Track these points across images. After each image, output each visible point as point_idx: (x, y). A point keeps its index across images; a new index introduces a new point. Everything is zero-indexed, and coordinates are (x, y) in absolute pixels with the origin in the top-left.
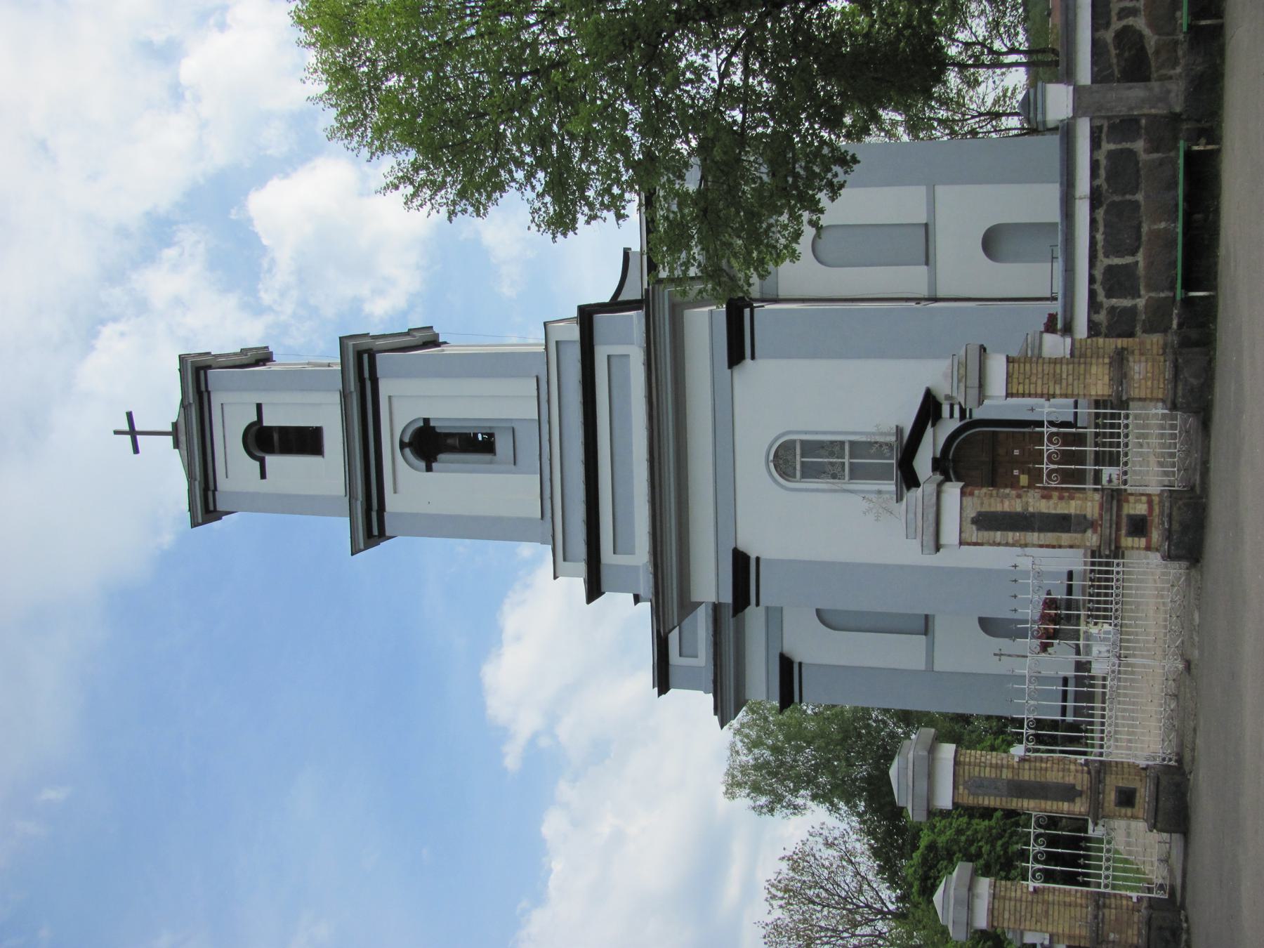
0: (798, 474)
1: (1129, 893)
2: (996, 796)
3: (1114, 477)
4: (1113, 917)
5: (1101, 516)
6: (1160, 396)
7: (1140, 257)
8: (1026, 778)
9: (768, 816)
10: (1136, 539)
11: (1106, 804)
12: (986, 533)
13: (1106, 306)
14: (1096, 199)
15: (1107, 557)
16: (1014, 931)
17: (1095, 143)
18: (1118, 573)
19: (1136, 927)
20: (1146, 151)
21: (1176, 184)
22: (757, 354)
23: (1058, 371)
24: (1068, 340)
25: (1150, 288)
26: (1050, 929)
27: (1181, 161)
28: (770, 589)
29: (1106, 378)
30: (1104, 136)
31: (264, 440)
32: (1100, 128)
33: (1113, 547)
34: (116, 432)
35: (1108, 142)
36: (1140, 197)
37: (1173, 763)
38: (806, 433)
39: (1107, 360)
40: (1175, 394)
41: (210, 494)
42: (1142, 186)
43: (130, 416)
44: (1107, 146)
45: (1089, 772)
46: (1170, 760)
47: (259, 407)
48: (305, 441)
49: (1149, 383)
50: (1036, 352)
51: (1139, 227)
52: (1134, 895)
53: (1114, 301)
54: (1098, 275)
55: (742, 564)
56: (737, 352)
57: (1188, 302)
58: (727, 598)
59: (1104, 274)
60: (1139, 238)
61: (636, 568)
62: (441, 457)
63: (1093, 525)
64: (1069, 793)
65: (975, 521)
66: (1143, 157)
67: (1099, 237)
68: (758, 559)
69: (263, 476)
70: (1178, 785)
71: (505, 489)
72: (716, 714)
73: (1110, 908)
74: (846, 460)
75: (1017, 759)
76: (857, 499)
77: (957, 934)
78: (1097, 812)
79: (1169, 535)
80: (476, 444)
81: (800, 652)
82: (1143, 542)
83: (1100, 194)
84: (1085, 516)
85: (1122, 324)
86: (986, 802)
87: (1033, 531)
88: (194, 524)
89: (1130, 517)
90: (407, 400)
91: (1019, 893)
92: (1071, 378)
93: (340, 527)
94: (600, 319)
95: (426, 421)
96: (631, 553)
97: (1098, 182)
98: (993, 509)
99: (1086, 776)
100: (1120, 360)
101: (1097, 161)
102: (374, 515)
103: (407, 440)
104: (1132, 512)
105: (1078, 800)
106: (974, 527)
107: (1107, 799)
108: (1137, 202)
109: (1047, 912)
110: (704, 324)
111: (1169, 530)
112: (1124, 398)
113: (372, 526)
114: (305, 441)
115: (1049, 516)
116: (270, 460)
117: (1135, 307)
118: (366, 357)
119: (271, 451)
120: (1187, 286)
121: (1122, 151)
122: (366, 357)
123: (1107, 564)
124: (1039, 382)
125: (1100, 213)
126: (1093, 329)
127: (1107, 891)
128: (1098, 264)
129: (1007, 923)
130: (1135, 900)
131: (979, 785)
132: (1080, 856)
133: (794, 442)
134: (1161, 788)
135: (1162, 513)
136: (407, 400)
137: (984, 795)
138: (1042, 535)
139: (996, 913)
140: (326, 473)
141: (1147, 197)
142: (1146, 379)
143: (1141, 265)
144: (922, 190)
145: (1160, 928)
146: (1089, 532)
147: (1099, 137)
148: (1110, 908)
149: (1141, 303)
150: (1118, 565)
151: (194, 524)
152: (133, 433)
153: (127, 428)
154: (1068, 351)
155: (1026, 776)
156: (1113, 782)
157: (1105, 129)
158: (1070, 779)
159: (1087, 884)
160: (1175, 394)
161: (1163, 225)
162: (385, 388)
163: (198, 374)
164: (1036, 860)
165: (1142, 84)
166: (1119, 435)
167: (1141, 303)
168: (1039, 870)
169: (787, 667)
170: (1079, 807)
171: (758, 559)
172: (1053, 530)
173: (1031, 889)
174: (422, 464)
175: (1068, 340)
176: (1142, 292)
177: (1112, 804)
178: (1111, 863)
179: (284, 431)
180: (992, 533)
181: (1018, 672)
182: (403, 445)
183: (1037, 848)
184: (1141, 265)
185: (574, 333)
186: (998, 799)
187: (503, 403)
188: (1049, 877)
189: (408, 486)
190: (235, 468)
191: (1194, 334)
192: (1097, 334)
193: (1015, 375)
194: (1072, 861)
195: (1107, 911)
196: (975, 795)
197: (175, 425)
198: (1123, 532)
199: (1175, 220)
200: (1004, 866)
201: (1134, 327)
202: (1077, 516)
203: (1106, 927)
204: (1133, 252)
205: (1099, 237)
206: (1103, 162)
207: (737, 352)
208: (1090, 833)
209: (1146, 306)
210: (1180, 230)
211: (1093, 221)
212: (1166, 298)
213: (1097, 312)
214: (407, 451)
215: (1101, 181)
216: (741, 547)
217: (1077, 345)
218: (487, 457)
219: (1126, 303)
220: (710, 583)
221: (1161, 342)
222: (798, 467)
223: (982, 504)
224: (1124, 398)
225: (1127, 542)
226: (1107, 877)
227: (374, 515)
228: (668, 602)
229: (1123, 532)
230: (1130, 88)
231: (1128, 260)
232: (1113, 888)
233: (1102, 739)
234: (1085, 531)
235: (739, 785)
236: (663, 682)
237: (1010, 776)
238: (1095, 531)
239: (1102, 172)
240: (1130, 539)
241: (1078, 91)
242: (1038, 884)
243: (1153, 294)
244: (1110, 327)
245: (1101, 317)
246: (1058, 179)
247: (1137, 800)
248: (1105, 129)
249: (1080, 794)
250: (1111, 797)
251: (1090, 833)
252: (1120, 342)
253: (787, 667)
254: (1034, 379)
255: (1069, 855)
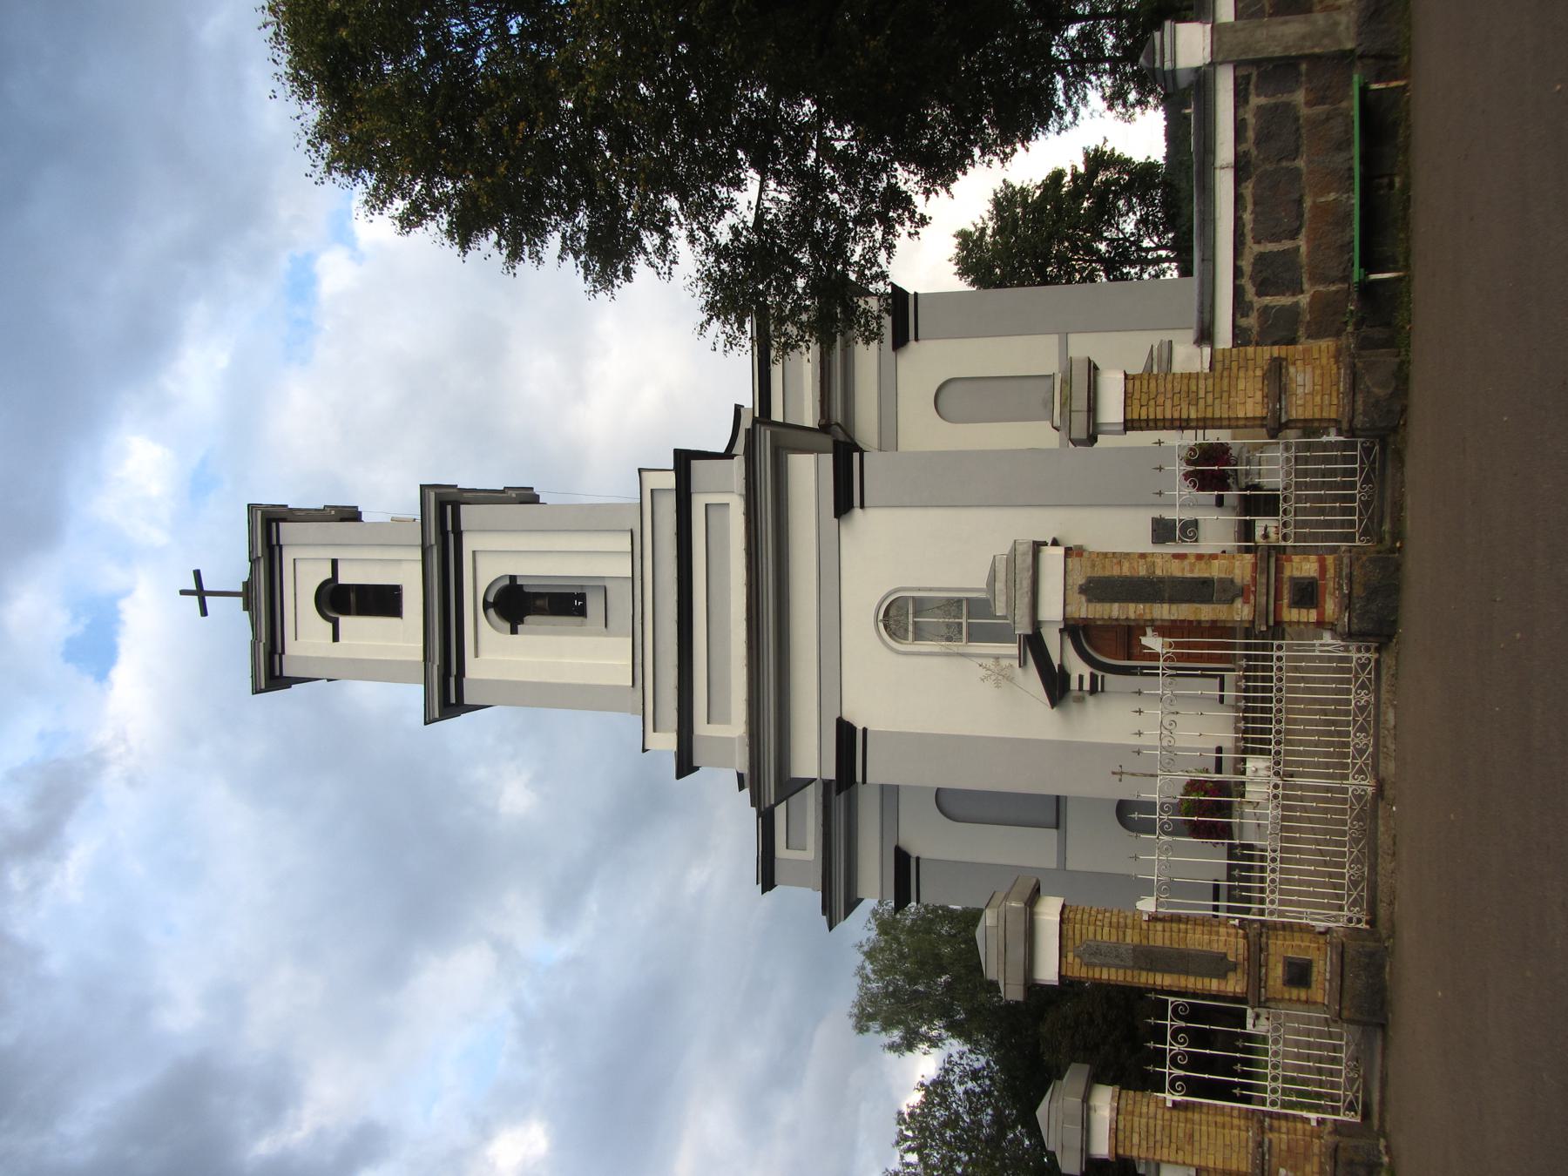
0: (910, 635)
1: (1305, 1114)
2: (1118, 967)
3: (1272, 531)
4: (1284, 1147)
5: (1254, 579)
6: (1333, 416)
7: (1302, 243)
8: (1159, 943)
9: (908, 1054)
10: (1304, 611)
11: (1271, 982)
12: (1099, 606)
13: (1256, 306)
14: (1241, 169)
15: (1263, 635)
16: (1147, 1162)
17: (1240, 97)
18: (1279, 659)
19: (1316, 1160)
20: (1309, 104)
21: (1349, 143)
22: (866, 503)
23: (1194, 388)
24: (1207, 351)
25: (1315, 279)
26: (1196, 1161)
27: (1356, 113)
28: (879, 769)
29: (1259, 395)
30: (1252, 87)
31: (338, 600)
32: (1248, 78)
33: (1271, 623)
34: (183, 592)
35: (1258, 95)
36: (1301, 163)
37: (1363, 926)
38: (919, 590)
39: (1259, 373)
40: (1354, 410)
41: (277, 657)
42: (1304, 148)
43: (197, 574)
44: (1255, 101)
45: (1246, 937)
46: (1359, 921)
47: (335, 563)
48: (383, 601)
49: (1318, 399)
50: (1164, 365)
51: (1300, 202)
52: (1313, 1116)
53: (1267, 300)
54: (1246, 265)
55: (847, 737)
56: (845, 501)
57: (1367, 289)
58: (831, 774)
59: (1254, 265)
60: (1300, 215)
61: (730, 740)
62: (528, 619)
63: (1243, 593)
64: (1218, 965)
65: (1083, 590)
66: (1304, 111)
67: (1247, 217)
68: (865, 730)
69: (336, 638)
70: (1371, 955)
71: (591, 656)
72: (824, 913)
73: (1279, 1131)
74: (964, 621)
75: (1146, 917)
76: (972, 664)
77: (1070, 1162)
78: (1257, 995)
79: (1348, 603)
80: (565, 603)
81: (916, 846)
82: (1313, 615)
83: (1248, 162)
84: (1232, 581)
85: (1281, 329)
86: (1105, 976)
87: (1162, 601)
88: (256, 690)
89: (1292, 579)
90: (492, 555)
91: (1152, 1108)
92: (1210, 396)
93: (413, 695)
94: (696, 465)
95: (513, 578)
96: (725, 728)
97: (1243, 147)
98: (1107, 574)
99: (1241, 942)
100: (1276, 374)
101: (1244, 120)
102: (452, 680)
103: (491, 599)
104: (1296, 574)
105: (1231, 975)
106: (1083, 598)
107: (1271, 974)
108: (1297, 169)
109: (1192, 1136)
110: (808, 475)
111: (1350, 595)
112: (1284, 420)
113: (449, 696)
114: (383, 601)
115: (1183, 581)
116: (344, 621)
117: (1297, 304)
118: (449, 508)
119: (347, 612)
120: (1369, 264)
121: (1276, 106)
122: (449, 508)
123: (1264, 647)
124: (1168, 404)
125: (1248, 189)
126: (1239, 335)
127: (1276, 1109)
128: (1247, 251)
129: (1136, 1149)
130: (1314, 1123)
131: (1094, 954)
132: (1236, 1085)
133: (906, 598)
134: (1347, 960)
135: (1338, 574)
136: (492, 555)
137: (1102, 966)
138: (1174, 607)
139: (1121, 1136)
140: (402, 637)
141: (1310, 162)
142: (1312, 394)
143: (1303, 249)
144: (1053, 340)
145: (1351, 1163)
146: (1238, 603)
147: (1246, 89)
148: (1279, 1131)
149: (1304, 300)
150: (1280, 648)
151: (256, 690)
152: (200, 593)
153: (194, 587)
154: (1207, 365)
155: (1160, 938)
156: (1280, 949)
157: (1254, 78)
158: (1218, 947)
159: (1248, 1100)
160: (1354, 410)
161: (1332, 196)
162: (470, 543)
163: (269, 525)
164: (1174, 1064)
165: (1301, 17)
166: (1270, 700)
167: (1304, 300)
168: (1179, 1078)
169: (903, 864)
170: (1234, 985)
171: (865, 730)
172: (1190, 601)
173: (1169, 1104)
174: (507, 626)
175: (1207, 351)
176: (1306, 286)
177: (1279, 981)
178: (1280, 1071)
179: (362, 590)
180: (1107, 606)
181: (1145, 796)
182: (486, 605)
183: (1176, 1047)
184: (1303, 249)
185: (669, 480)
186: (1121, 972)
187: (596, 559)
188: (1194, 1088)
189: (494, 653)
190: (307, 634)
191: (1378, 333)
192: (1246, 343)
193: (1137, 396)
194: (1227, 1066)
195: (1274, 1136)
196: (1089, 965)
197: (246, 585)
198: (1286, 601)
199: (1350, 190)
200: (1131, 1069)
201: (1296, 331)
202: (1221, 580)
203: (1274, 1160)
204: (1293, 235)
205: (1247, 217)
206: (1251, 120)
207: (845, 501)
208: (1250, 1028)
209: (1311, 304)
210: (1356, 201)
211: (1238, 198)
212: (1337, 292)
213: (1245, 315)
214: (491, 612)
215: (1249, 145)
216: (846, 717)
217: (1219, 357)
218: (579, 619)
219: (1285, 300)
220: (812, 757)
221: (1332, 349)
222: (911, 628)
223: (1093, 566)
224: (1284, 420)
225: (1291, 615)
226: (1274, 1091)
227: (452, 680)
228: (768, 781)
229: (1286, 601)
230: (1286, 22)
231: (1287, 245)
232: (1283, 1107)
233: (1262, 890)
234: (1232, 601)
235: (871, 1017)
236: (767, 881)
237: (1136, 940)
238: (1246, 602)
239: (1251, 134)
240: (1295, 611)
241: (1217, 31)
242: (1178, 1098)
243: (1321, 288)
244: (1260, 334)
245: (1251, 321)
246: (1195, 326)
247: (1314, 978)
248: (1254, 78)
249: (1234, 967)
250: (1277, 972)
251: (1250, 1028)
252: (1276, 351)
253: (903, 864)
254: (1160, 400)
255: (1222, 1068)
